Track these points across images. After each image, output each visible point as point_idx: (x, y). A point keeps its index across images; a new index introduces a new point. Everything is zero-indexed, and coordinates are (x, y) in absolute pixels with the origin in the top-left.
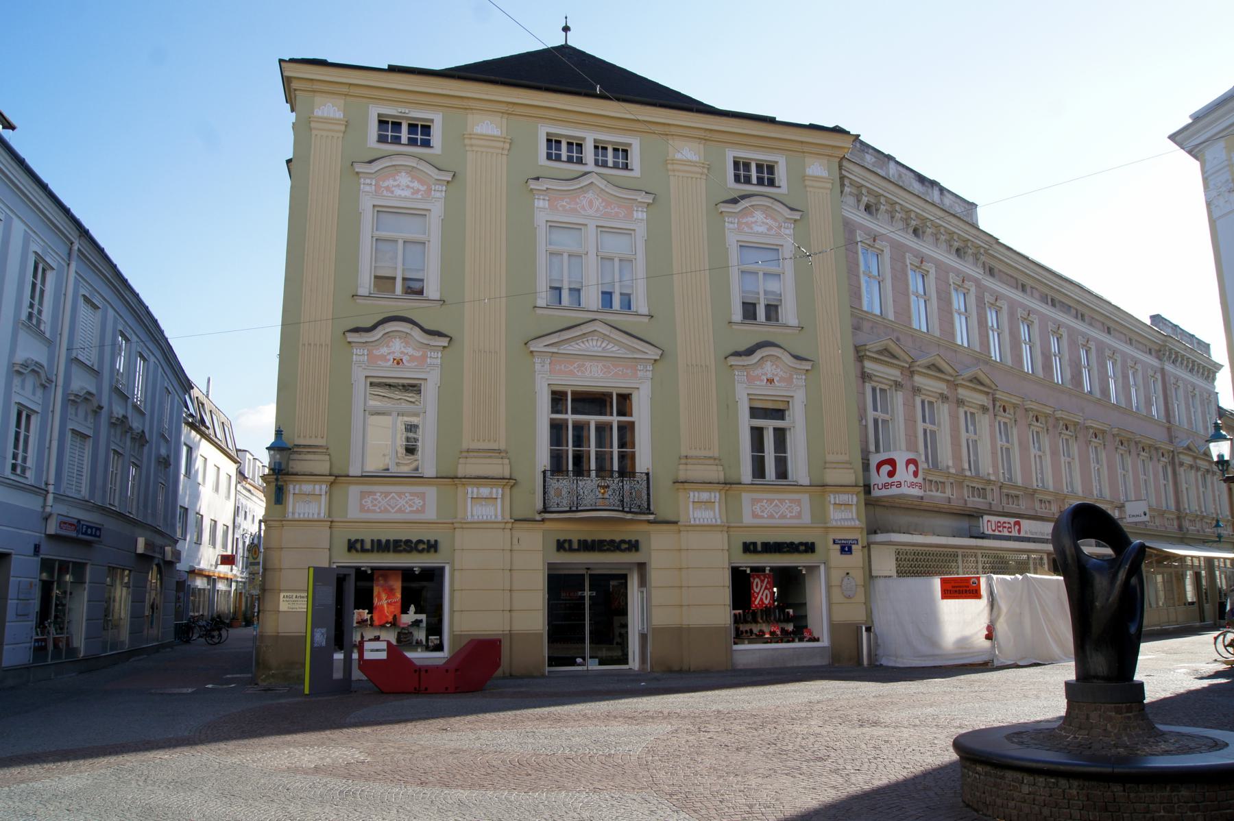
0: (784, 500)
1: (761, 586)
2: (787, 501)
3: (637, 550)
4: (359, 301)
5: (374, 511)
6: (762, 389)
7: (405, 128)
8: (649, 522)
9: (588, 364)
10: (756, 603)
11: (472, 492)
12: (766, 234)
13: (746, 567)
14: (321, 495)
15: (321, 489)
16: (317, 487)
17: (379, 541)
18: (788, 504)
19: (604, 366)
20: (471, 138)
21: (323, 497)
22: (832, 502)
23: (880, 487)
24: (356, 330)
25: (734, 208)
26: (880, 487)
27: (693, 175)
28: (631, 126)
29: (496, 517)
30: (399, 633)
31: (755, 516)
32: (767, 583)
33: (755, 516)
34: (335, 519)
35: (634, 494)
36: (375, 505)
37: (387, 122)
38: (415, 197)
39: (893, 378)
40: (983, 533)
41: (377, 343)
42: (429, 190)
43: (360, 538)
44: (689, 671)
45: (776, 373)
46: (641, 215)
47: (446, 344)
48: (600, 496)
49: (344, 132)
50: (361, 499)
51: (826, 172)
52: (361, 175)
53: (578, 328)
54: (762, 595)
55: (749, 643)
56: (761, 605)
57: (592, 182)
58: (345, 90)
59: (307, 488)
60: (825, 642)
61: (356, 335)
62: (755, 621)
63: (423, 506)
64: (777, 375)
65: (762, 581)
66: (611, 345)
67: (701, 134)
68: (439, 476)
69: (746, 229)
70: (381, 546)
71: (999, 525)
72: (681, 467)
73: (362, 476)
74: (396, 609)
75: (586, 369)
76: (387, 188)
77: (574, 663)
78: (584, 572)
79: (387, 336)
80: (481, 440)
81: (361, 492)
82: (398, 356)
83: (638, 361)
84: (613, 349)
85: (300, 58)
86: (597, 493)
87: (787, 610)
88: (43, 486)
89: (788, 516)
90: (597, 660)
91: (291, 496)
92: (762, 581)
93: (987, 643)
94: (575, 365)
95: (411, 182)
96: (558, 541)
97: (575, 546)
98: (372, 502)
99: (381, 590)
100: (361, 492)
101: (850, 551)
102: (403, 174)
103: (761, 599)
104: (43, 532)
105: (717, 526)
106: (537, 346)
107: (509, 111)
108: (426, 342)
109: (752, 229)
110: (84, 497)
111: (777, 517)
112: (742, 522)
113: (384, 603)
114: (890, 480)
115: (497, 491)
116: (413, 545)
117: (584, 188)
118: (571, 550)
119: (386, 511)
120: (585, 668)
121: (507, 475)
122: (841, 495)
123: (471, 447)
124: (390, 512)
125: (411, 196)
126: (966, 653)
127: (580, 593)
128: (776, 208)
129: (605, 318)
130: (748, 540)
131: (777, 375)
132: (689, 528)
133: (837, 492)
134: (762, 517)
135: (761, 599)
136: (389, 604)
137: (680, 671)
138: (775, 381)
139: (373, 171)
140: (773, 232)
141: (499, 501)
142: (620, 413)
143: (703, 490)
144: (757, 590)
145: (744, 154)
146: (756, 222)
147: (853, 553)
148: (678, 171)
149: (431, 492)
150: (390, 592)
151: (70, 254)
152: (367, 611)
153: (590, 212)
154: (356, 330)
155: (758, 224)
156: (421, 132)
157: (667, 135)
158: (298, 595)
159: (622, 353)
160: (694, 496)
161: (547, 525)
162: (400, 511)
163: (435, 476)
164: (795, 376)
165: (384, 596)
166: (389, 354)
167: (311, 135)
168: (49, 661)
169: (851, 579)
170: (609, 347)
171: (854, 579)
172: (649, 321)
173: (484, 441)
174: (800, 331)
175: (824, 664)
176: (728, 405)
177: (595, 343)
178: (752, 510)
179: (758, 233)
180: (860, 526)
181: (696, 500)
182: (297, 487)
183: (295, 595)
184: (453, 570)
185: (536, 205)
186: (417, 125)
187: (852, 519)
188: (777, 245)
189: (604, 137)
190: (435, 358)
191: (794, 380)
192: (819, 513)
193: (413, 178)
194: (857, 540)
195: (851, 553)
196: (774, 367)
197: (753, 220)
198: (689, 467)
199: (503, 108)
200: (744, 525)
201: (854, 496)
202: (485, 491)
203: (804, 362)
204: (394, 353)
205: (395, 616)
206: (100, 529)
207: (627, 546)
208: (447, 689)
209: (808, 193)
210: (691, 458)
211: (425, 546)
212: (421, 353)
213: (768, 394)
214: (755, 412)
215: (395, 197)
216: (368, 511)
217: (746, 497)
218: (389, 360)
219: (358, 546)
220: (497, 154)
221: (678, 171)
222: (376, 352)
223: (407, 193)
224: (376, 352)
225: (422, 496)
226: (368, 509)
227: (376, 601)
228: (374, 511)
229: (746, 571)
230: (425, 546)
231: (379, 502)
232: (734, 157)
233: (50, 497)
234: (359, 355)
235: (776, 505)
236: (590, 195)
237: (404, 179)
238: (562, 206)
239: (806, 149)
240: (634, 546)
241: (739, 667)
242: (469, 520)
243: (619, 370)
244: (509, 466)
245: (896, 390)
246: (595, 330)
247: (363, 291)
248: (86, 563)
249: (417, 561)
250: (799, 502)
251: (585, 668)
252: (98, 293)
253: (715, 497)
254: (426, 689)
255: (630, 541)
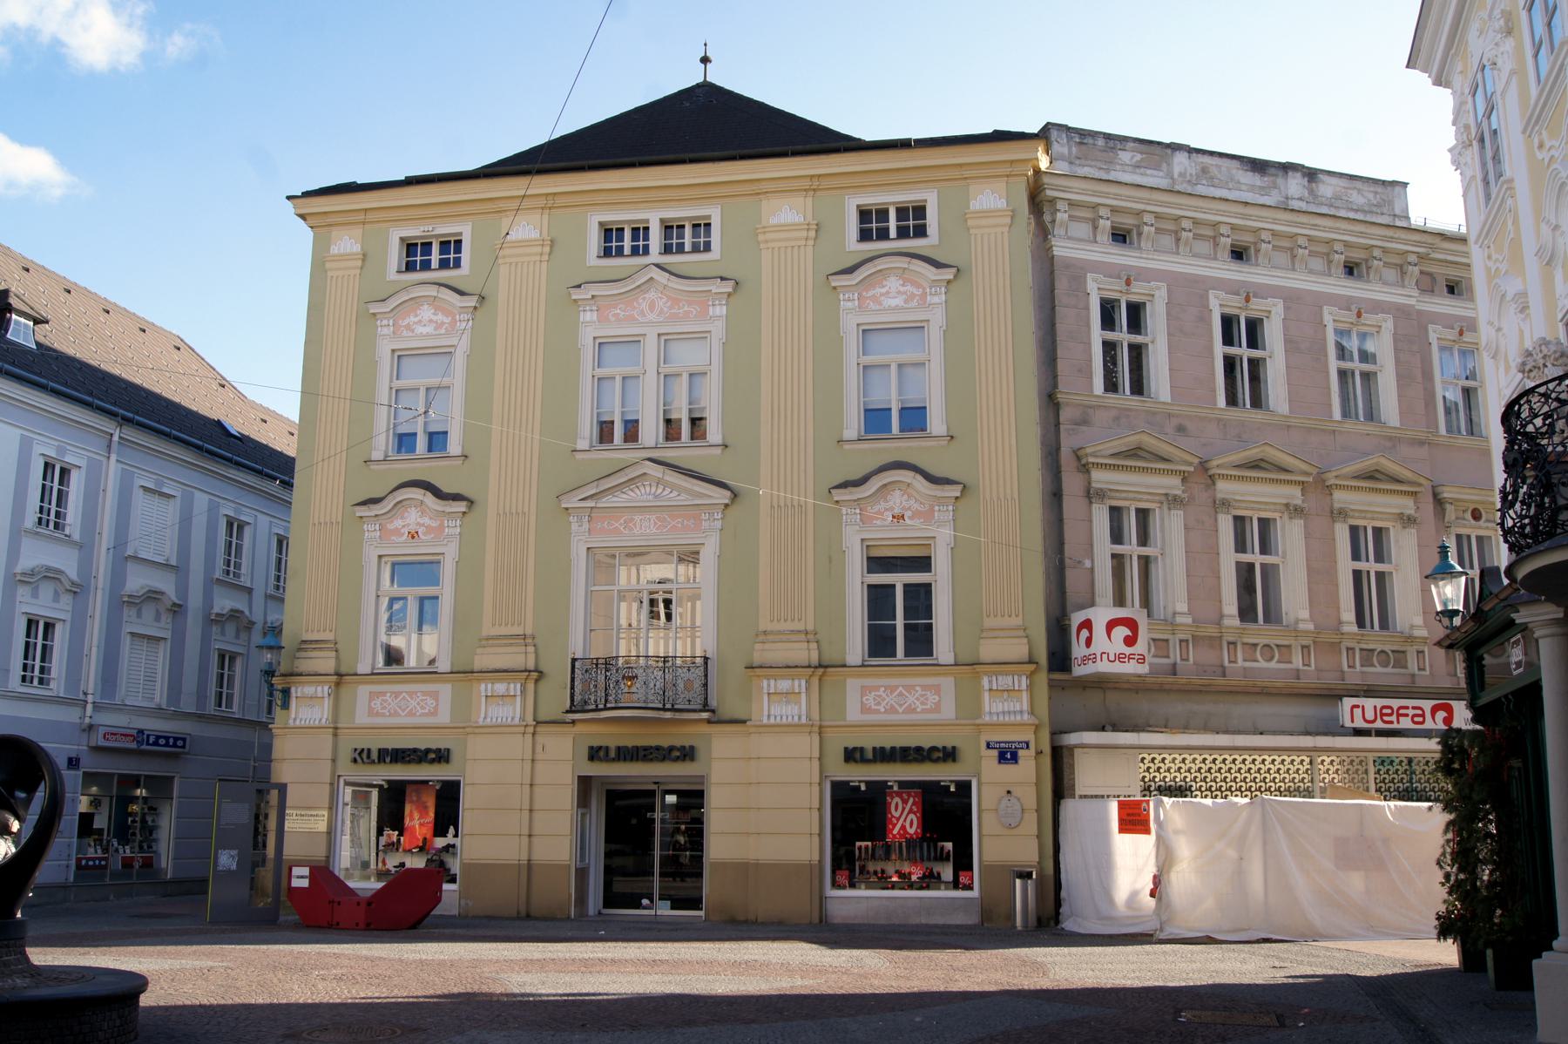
0: (913, 687)
1: (904, 809)
2: (918, 688)
3: (447, 761)
4: (374, 467)
5: (383, 715)
6: (402, 548)
7: (435, 249)
8: (709, 721)
9: (637, 518)
10: (895, 832)
11: (486, 690)
12: (903, 308)
13: (860, 782)
14: (800, 693)
15: (323, 691)
16: (319, 689)
17: (883, 749)
18: (920, 692)
19: (657, 518)
20: (764, 233)
21: (326, 700)
22: (987, 687)
23: (1112, 658)
24: (845, 485)
25: (849, 280)
26: (1112, 658)
27: (793, 243)
28: (705, 192)
29: (800, 718)
30: (428, 860)
31: (865, 709)
32: (913, 804)
33: (865, 709)
34: (339, 725)
35: (592, 686)
36: (384, 708)
37: (672, 227)
38: (437, 332)
39: (1163, 492)
40: (1342, 726)
41: (389, 515)
42: (454, 322)
43: (858, 745)
44: (755, 922)
45: (907, 506)
46: (720, 310)
47: (958, 494)
48: (626, 690)
49: (362, 268)
50: (370, 702)
51: (1004, 201)
52: (378, 316)
53: (622, 473)
54: (905, 821)
55: (867, 888)
56: (902, 836)
57: (652, 278)
58: (361, 217)
59: (309, 690)
60: (974, 894)
61: (363, 508)
62: (887, 858)
63: (436, 708)
64: (909, 508)
65: (905, 802)
66: (675, 493)
67: (806, 184)
68: (455, 670)
69: (872, 306)
70: (885, 755)
71: (1381, 713)
72: (758, 646)
73: (373, 674)
74: (427, 831)
75: (635, 525)
76: (408, 327)
77: (638, 906)
78: (654, 787)
79: (400, 506)
80: (1013, 615)
81: (862, 687)
82: (413, 528)
83: (702, 507)
84: (671, 497)
85: (317, 188)
86: (622, 686)
87: (940, 844)
88: (82, 697)
89: (918, 710)
90: (669, 902)
91: (986, 695)
92: (905, 802)
93: (1152, 902)
94: (622, 521)
95: (434, 314)
96: (591, 748)
97: (870, 755)
98: (927, 699)
99: (414, 807)
100: (862, 687)
101: (1014, 758)
102: (426, 307)
103: (903, 827)
104: (85, 743)
105: (802, 725)
106: (572, 502)
107: (550, 203)
108: (440, 509)
109: (880, 304)
110: (160, 705)
111: (901, 711)
112: (845, 720)
113: (416, 823)
114: (1128, 650)
115: (515, 687)
116: (925, 753)
117: (643, 288)
118: (864, 760)
119: (396, 714)
120: (652, 912)
121: (531, 665)
122: (1000, 678)
123: (769, 629)
124: (400, 715)
125: (434, 333)
126: (1137, 917)
127: (649, 814)
128: (918, 269)
129: (663, 455)
130: (851, 745)
131: (909, 508)
132: (761, 730)
133: (997, 674)
134: (878, 712)
135: (903, 827)
136: (421, 825)
137: (746, 922)
138: (906, 518)
139: (388, 310)
140: (914, 303)
141: (518, 699)
142: (1251, 566)
143: (783, 677)
144: (897, 814)
145: (872, 199)
146: (888, 293)
147: (1020, 762)
148: (773, 240)
149: (445, 690)
150: (423, 810)
151: (109, 446)
152: (397, 833)
153: (652, 317)
154: (845, 485)
155: (890, 295)
156: (913, 220)
157: (758, 194)
158: (299, 812)
159: (684, 499)
160: (769, 685)
161: (579, 728)
162: (411, 714)
163: (449, 671)
164: (937, 508)
165: (416, 816)
166: (404, 526)
167: (326, 277)
168: (108, 881)
169: (1014, 801)
170: (665, 493)
171: (1019, 799)
172: (722, 453)
173: (506, 625)
174: (949, 441)
175: (970, 923)
176: (830, 559)
177: (648, 489)
178: (862, 702)
179: (422, 335)
180: (1030, 722)
181: (772, 691)
182: (299, 690)
183: (295, 812)
184: (979, 784)
185: (581, 320)
186: (639, 228)
187: (1021, 712)
188: (922, 321)
189: (673, 213)
190: (453, 528)
191: (936, 514)
192: (969, 704)
193: (437, 309)
194: (1027, 744)
195: (1016, 762)
196: (906, 497)
197: (884, 290)
198: (767, 646)
199: (542, 202)
200: (847, 723)
201: (1024, 678)
202: (500, 688)
203: (947, 487)
204: (409, 525)
205: (425, 839)
206: (184, 740)
207: (678, 754)
208: (357, 924)
209: (973, 237)
210: (772, 632)
211: (941, 755)
212: (438, 522)
213: (893, 537)
214: (877, 564)
215: (417, 336)
216: (378, 714)
217: (853, 685)
218: (403, 534)
219: (858, 755)
220: (535, 262)
221: (510, 256)
222: (391, 526)
223: (429, 329)
224: (391, 526)
225: (435, 695)
226: (870, 708)
227: (407, 821)
228: (383, 715)
229: (859, 786)
230: (941, 755)
231: (390, 704)
232: (858, 206)
233: (89, 707)
234: (371, 531)
235: (901, 694)
236: (652, 295)
237: (426, 312)
238: (614, 315)
239: (967, 173)
240: (687, 754)
241: (836, 921)
242: (481, 723)
243: (678, 523)
244: (817, 652)
245: (1169, 509)
246: (645, 474)
247: (377, 455)
248: (173, 777)
249: (943, 774)
250: (937, 689)
251: (652, 912)
252: (196, 488)
253: (800, 686)
254: (338, 924)
255: (684, 747)
